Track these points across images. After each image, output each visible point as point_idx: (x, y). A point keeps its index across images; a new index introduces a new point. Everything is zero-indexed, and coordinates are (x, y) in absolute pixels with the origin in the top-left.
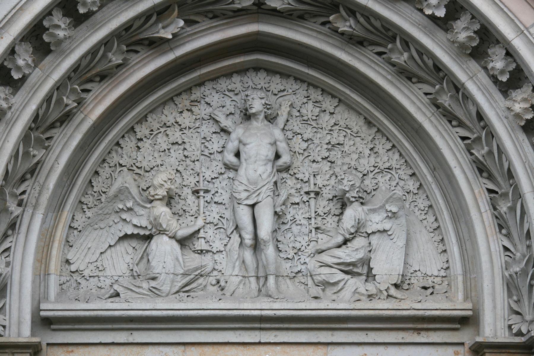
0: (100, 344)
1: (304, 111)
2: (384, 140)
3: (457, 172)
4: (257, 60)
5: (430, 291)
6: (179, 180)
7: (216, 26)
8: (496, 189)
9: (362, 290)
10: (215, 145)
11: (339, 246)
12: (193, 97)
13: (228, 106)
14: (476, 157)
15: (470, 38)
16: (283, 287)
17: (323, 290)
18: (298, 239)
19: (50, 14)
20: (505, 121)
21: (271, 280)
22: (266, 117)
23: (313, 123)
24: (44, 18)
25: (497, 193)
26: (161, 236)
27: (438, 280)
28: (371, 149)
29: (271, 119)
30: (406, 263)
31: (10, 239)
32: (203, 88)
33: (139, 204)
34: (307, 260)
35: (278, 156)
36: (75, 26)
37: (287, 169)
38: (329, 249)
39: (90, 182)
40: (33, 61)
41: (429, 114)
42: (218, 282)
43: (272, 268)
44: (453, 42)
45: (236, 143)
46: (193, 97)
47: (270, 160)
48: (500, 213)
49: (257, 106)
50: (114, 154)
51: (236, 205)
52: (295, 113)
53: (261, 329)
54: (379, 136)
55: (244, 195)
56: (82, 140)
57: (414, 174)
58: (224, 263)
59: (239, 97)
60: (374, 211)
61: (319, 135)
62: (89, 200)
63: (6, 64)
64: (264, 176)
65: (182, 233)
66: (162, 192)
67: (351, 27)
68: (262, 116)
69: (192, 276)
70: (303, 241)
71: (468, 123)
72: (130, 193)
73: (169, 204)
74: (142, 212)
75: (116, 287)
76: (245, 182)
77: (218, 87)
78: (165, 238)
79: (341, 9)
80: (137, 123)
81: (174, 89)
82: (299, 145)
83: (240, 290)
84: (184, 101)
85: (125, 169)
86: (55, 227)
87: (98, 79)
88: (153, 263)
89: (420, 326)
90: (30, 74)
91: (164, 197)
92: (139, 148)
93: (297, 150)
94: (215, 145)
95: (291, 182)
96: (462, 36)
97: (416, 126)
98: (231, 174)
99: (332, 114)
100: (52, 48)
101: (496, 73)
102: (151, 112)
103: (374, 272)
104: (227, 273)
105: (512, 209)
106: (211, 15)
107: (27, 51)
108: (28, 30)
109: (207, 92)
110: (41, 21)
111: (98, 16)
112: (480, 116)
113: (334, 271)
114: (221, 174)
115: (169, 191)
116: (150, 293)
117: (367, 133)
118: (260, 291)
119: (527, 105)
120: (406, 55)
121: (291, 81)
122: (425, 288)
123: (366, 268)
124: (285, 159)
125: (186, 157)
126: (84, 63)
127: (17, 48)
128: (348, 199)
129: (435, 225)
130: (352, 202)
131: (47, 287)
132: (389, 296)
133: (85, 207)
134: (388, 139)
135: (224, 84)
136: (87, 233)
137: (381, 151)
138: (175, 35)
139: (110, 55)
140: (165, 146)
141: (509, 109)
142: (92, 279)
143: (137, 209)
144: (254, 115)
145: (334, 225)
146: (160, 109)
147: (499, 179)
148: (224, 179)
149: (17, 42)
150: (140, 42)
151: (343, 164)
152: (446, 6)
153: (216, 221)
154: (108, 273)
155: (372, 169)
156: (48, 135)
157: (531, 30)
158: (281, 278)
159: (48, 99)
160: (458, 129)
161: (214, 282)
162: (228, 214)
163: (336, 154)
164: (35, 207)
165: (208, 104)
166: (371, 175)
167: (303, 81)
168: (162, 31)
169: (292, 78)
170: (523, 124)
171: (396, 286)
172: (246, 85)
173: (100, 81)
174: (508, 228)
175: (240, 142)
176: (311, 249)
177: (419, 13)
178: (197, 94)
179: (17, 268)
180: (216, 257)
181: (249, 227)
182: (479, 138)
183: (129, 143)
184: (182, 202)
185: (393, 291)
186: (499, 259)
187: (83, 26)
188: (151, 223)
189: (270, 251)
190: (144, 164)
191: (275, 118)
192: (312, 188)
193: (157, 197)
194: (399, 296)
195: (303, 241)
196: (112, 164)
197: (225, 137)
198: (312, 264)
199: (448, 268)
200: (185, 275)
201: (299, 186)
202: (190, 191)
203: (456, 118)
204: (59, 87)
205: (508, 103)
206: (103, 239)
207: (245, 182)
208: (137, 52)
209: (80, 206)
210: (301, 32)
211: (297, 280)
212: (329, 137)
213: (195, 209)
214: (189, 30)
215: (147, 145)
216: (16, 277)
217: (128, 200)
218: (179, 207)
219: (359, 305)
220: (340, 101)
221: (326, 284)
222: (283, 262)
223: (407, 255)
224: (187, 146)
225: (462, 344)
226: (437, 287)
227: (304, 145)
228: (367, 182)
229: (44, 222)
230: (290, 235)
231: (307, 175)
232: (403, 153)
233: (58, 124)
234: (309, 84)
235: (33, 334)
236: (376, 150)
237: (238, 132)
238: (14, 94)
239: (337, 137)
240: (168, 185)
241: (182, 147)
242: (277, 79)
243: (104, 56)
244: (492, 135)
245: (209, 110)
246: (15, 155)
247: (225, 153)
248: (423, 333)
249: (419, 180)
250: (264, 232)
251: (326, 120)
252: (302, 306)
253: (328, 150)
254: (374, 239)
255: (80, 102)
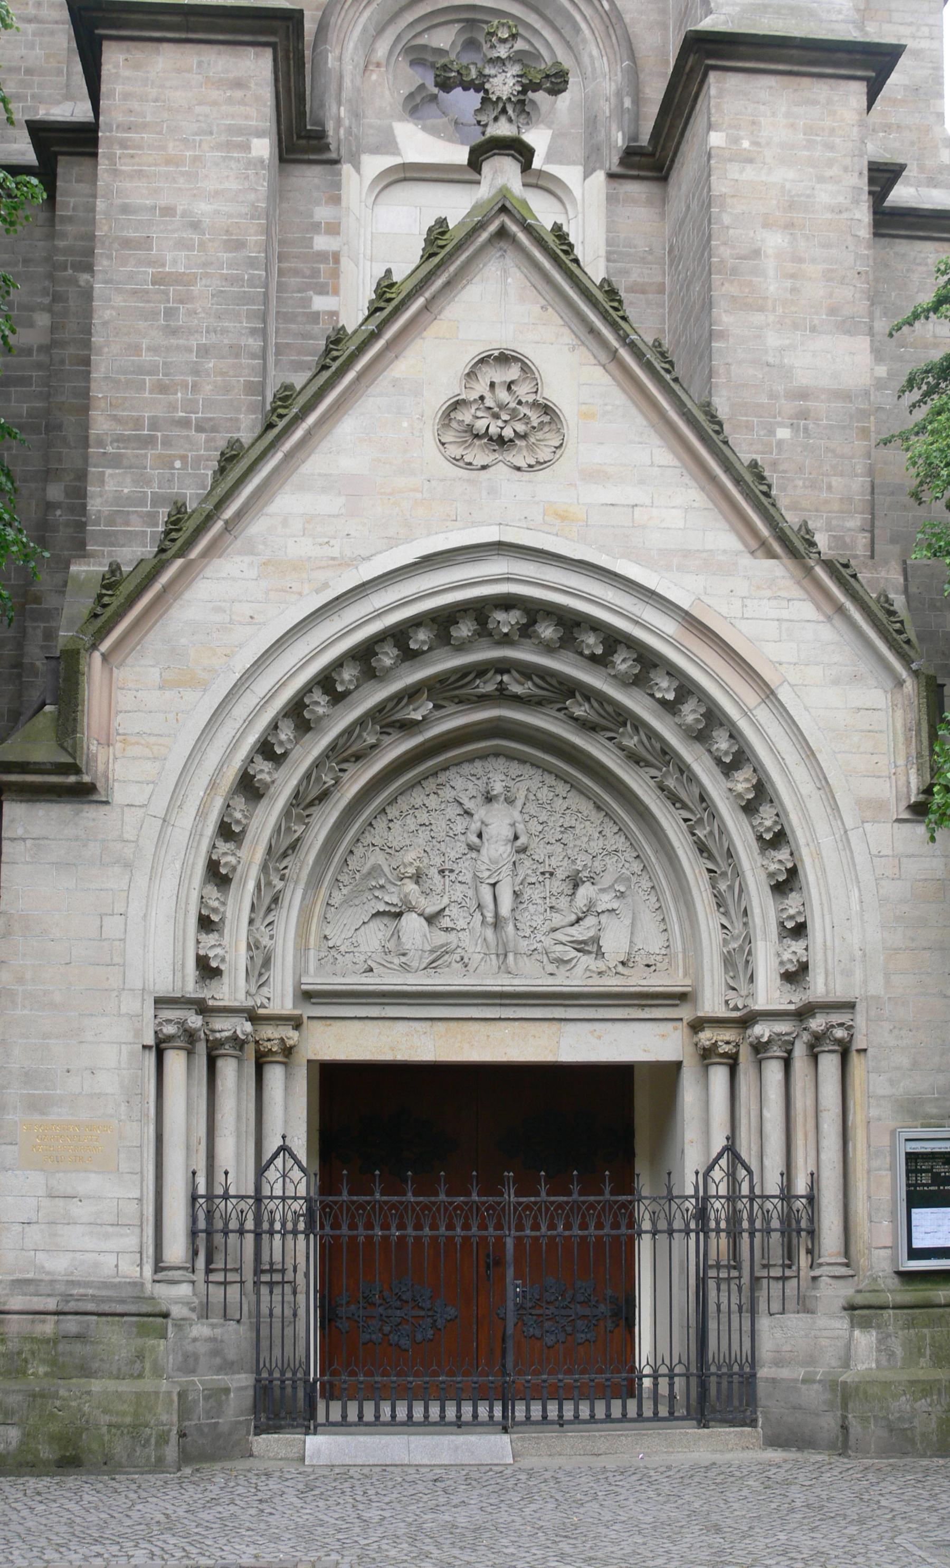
0: (355, 1018)
1: (539, 795)
2: (611, 824)
3: (680, 852)
4: (497, 745)
5: (653, 968)
6: (426, 860)
7: (461, 711)
8: (715, 869)
9: (593, 967)
10: (459, 828)
11: (572, 925)
12: (439, 781)
13: (470, 789)
14: (699, 837)
15: (697, 720)
16: (521, 964)
17: (557, 967)
18: (534, 917)
19: (310, 691)
20: (727, 801)
21: (511, 957)
22: (505, 799)
23: (548, 807)
24: (305, 694)
25: (715, 872)
26: (410, 913)
27: (659, 958)
28: (600, 832)
29: (510, 801)
30: (631, 942)
31: (273, 913)
32: (448, 772)
33: (390, 882)
34: (543, 938)
35: (516, 838)
36: (334, 705)
37: (523, 850)
38: (563, 927)
39: (346, 860)
40: (295, 737)
41: (655, 797)
42: (462, 959)
43: (511, 945)
44: (680, 726)
45: (479, 824)
46: (439, 781)
47: (509, 841)
48: (719, 892)
49: (498, 788)
50: (367, 834)
51: (479, 884)
52: (532, 797)
53: (501, 1005)
54: (607, 820)
55: (487, 874)
56: (338, 818)
57: (638, 857)
58: (467, 941)
59: (481, 781)
60: (603, 890)
61: (553, 819)
62: (344, 878)
63: (269, 739)
64: (505, 856)
65: (430, 910)
66: (411, 870)
67: (585, 711)
68: (502, 798)
69: (438, 953)
70: (539, 920)
71: (690, 804)
72: (382, 870)
73: (417, 883)
74: (393, 890)
75: (369, 962)
76: (487, 861)
77: (462, 771)
78: (414, 915)
79: (577, 694)
80: (388, 804)
81: (423, 772)
82: (535, 827)
83: (481, 968)
84: (430, 785)
85: (377, 848)
86: (314, 903)
87: (353, 759)
88: (403, 940)
89: (644, 1002)
90: (292, 749)
91: (413, 874)
92: (389, 828)
93: (533, 832)
94: (460, 825)
95: (528, 863)
96: (690, 719)
97: (642, 809)
98: (474, 855)
99: (565, 798)
100: (312, 725)
101: (720, 754)
102: (400, 794)
103: (603, 950)
104: (471, 950)
105: (731, 887)
106: (456, 700)
107: (289, 727)
108: (290, 706)
109: (451, 777)
110: (302, 698)
111: (355, 695)
112: (703, 798)
113: (568, 948)
114: (465, 854)
115: (418, 869)
116: (400, 969)
117: (597, 817)
118: (499, 968)
119: (749, 786)
120: (636, 738)
121: (528, 766)
122: (648, 966)
123: (595, 945)
124: (522, 840)
125: (433, 838)
126: (341, 741)
127: (280, 724)
128: (581, 879)
129: (657, 905)
130: (584, 882)
131: (307, 961)
132: (617, 973)
133: (341, 884)
134: (615, 823)
135: (467, 769)
136: (343, 910)
137: (609, 835)
138: (424, 718)
139: (365, 734)
140: (413, 828)
141: (730, 790)
142: (347, 955)
143: (388, 886)
144: (496, 796)
145: (567, 905)
146: (409, 792)
147: (719, 859)
148: (467, 859)
149: (280, 717)
150: (391, 725)
151: (575, 846)
152: (675, 690)
153: (459, 900)
154: (362, 948)
155: (601, 851)
156: (307, 812)
157: (754, 712)
158: (519, 956)
159: (308, 776)
160: (681, 811)
161: (458, 959)
162: (470, 893)
163: (568, 837)
164: (296, 883)
165: (453, 788)
166: (600, 857)
167: (538, 767)
168: (413, 713)
169: (528, 764)
170: (743, 804)
171: (623, 963)
172: (487, 770)
173: (355, 762)
174: (726, 906)
175: (483, 822)
176: (546, 928)
177: (649, 698)
178: (442, 778)
179: (280, 942)
180: (460, 934)
181: (491, 906)
182: (701, 820)
183: (380, 824)
184: (430, 881)
185: (620, 968)
186: (719, 935)
187: (341, 705)
188: (401, 900)
189: (510, 928)
190: (395, 844)
191: (513, 801)
192: (547, 869)
193: (407, 875)
194: (626, 973)
195: (539, 920)
196: (365, 844)
197: (468, 819)
198: (548, 941)
199: (668, 946)
200: (432, 951)
201: (535, 867)
202: (436, 871)
203: (680, 800)
204: (317, 764)
205: (730, 785)
206: (357, 916)
207: (487, 861)
208: (389, 734)
209: (337, 883)
210: (544, 713)
211: (533, 957)
212: (562, 820)
213: (441, 888)
214: (438, 714)
215: (397, 826)
216: (279, 950)
217: (381, 877)
218: (427, 885)
219: (590, 982)
220: (572, 786)
221: (561, 962)
222: (521, 940)
223: (632, 933)
224: (433, 827)
225: (681, 1019)
226: (658, 964)
227: (540, 828)
228: (596, 864)
229: (303, 899)
230: (527, 914)
231: (543, 857)
232: (629, 836)
233: (317, 802)
234: (544, 770)
235: (295, 1007)
236: (603, 833)
237: (481, 813)
238: (276, 769)
239: (568, 821)
240: (417, 864)
241: (429, 828)
242: (515, 764)
243: (359, 736)
244: (714, 815)
245: (453, 793)
246: (278, 830)
247: (469, 834)
248: (646, 1009)
249: (642, 862)
250: (505, 910)
251: (559, 804)
252: (540, 982)
253: (562, 832)
254: (603, 918)
255: (337, 781)
